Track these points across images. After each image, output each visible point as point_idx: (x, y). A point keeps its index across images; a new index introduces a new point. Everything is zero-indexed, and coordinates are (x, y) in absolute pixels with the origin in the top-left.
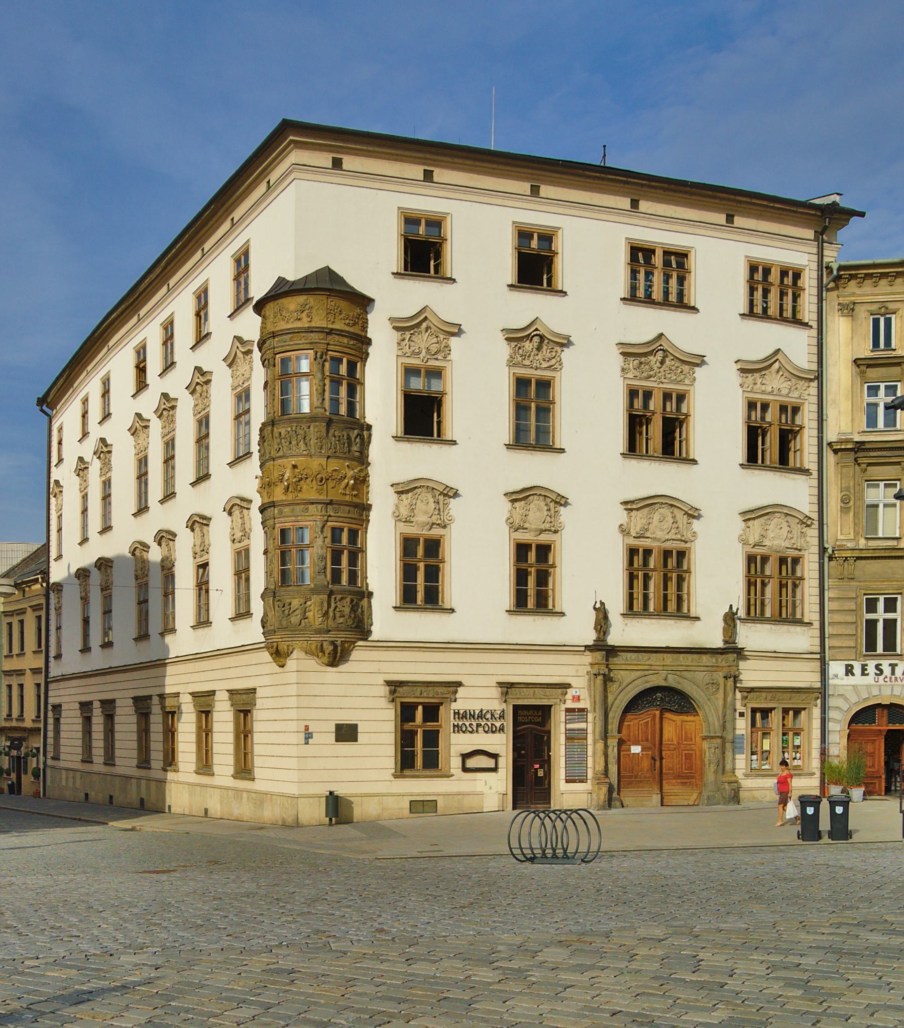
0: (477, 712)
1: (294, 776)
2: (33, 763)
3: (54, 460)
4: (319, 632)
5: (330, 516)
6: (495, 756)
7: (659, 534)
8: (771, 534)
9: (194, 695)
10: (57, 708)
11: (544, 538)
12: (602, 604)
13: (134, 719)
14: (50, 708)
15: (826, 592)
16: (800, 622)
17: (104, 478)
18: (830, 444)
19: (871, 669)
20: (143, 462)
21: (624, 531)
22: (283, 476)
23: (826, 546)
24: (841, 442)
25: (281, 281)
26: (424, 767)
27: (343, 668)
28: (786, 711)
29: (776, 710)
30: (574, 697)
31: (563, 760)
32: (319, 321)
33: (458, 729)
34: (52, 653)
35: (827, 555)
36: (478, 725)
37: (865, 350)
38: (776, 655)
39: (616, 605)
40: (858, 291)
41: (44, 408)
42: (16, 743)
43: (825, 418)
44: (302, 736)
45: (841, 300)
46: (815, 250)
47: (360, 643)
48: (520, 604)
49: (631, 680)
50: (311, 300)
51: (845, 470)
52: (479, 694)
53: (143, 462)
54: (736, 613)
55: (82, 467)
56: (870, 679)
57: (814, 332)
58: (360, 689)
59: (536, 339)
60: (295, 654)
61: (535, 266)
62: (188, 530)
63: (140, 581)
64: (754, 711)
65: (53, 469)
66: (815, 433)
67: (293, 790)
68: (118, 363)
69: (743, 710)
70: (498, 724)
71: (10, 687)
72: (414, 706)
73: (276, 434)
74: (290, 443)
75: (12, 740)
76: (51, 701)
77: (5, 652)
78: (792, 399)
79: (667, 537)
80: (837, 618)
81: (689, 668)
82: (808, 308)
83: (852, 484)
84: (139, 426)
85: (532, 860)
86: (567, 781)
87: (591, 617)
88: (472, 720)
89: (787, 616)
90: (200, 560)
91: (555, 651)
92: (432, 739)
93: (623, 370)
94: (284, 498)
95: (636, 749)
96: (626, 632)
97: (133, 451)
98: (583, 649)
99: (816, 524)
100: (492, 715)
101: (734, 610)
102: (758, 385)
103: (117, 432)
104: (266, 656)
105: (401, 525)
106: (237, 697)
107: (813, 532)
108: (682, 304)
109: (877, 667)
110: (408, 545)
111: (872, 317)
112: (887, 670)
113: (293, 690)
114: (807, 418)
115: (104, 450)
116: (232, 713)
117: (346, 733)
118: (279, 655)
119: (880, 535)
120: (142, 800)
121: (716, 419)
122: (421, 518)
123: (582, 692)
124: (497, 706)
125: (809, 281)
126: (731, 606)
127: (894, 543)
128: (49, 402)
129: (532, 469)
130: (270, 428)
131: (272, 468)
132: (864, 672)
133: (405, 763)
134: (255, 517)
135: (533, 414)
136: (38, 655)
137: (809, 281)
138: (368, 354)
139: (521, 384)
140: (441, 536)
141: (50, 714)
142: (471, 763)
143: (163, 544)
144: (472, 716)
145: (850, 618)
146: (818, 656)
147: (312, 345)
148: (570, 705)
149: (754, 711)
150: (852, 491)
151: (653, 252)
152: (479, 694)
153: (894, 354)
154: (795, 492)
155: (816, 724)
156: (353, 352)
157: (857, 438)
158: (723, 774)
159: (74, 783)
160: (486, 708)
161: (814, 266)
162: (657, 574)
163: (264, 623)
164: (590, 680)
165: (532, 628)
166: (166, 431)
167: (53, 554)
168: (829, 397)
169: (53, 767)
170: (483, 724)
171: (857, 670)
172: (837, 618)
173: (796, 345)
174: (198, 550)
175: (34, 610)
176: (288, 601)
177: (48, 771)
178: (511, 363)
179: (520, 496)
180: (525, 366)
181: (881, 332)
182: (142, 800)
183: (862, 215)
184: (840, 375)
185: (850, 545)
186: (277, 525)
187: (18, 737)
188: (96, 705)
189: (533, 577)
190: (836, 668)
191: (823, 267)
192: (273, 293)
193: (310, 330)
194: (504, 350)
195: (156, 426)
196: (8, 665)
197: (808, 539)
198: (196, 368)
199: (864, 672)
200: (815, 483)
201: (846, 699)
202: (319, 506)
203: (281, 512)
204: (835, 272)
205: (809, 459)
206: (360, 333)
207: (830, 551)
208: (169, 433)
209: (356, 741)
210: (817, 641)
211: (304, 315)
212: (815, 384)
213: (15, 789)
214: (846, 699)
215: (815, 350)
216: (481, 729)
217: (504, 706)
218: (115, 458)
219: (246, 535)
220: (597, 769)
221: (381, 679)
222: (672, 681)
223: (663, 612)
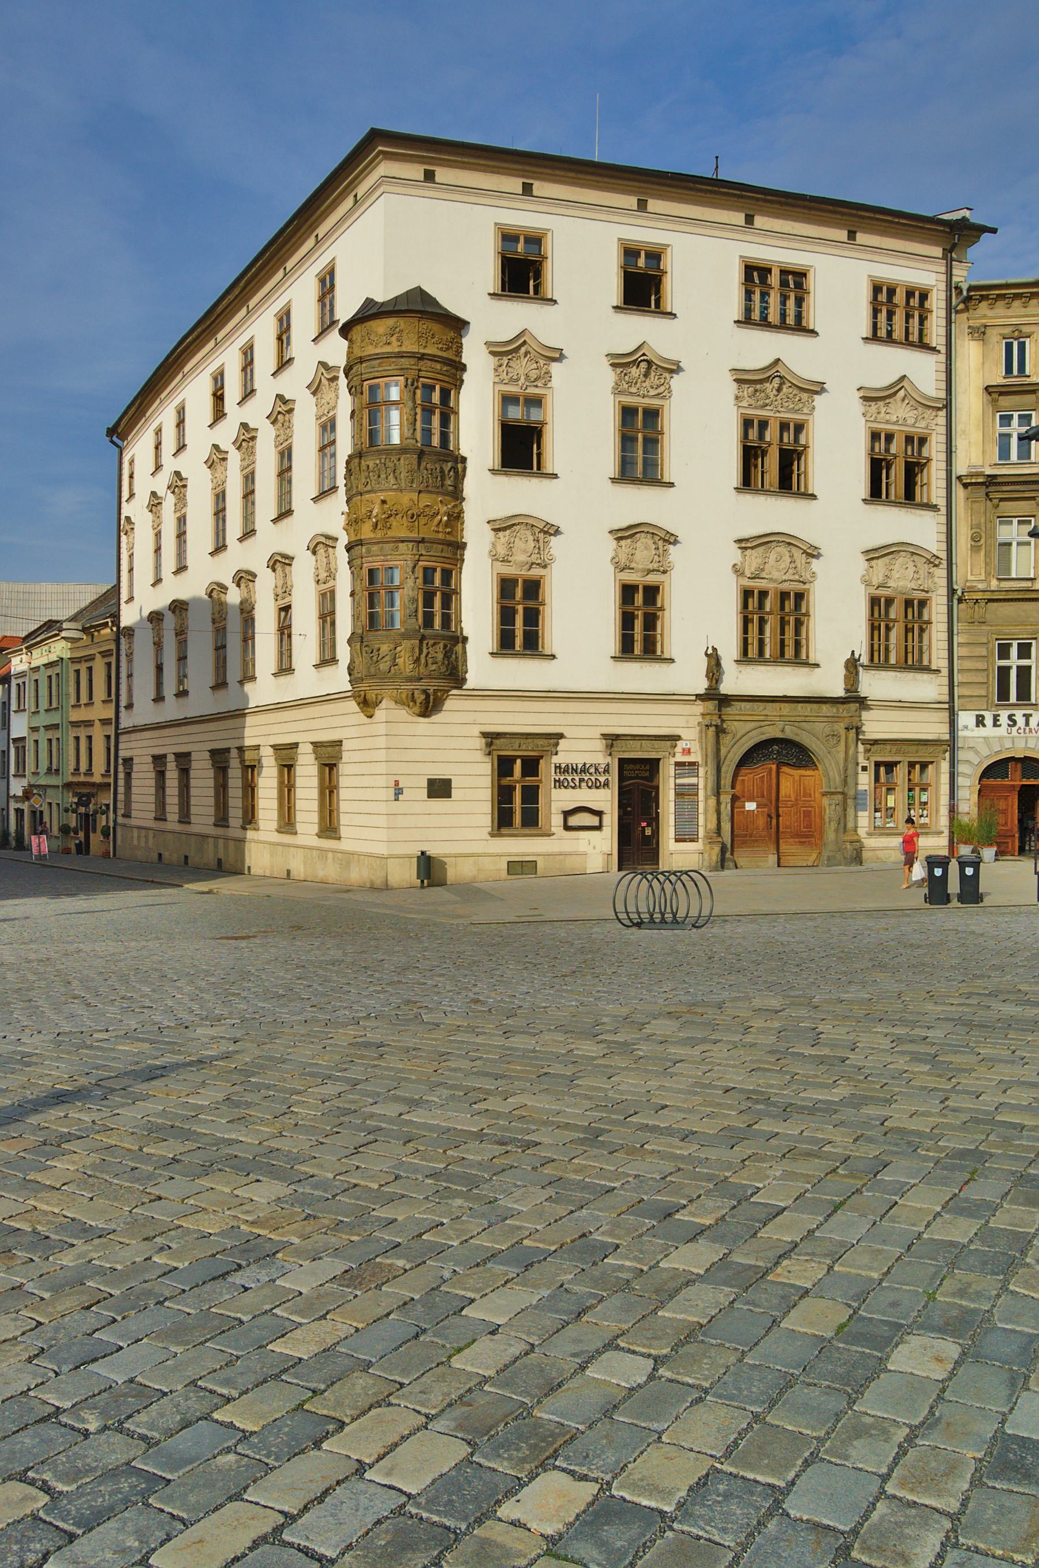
0: (580, 766)
2: (102, 821)
3: (125, 495)
4: (410, 679)
5: (421, 555)
6: (599, 814)
7: (776, 575)
10: (128, 761)
11: (652, 579)
12: (714, 649)
13: (211, 773)
14: (120, 761)
15: (955, 637)
16: (927, 669)
17: (178, 514)
18: (959, 478)
19: (1004, 720)
20: (220, 497)
21: (738, 571)
22: (371, 512)
23: (955, 587)
24: (971, 475)
25: (369, 302)
28: (912, 765)
29: (903, 764)
30: (684, 750)
31: (672, 817)
33: (559, 784)
34: (123, 703)
35: (956, 597)
36: (581, 780)
37: (997, 377)
38: (902, 704)
39: (729, 651)
40: (990, 313)
41: (115, 439)
43: (954, 449)
44: (392, 792)
45: (971, 323)
46: (943, 269)
47: (454, 692)
49: (745, 731)
50: (401, 323)
51: (975, 505)
52: (581, 747)
53: (220, 497)
54: (859, 660)
55: (155, 503)
56: (1002, 731)
57: (942, 358)
58: (454, 741)
59: (644, 365)
61: (642, 286)
62: (270, 570)
63: (217, 625)
64: (878, 765)
65: (124, 504)
67: (382, 849)
68: (193, 391)
69: (866, 763)
70: (602, 779)
73: (364, 468)
74: (379, 476)
75: (80, 796)
78: (919, 429)
79: (784, 578)
80: (968, 664)
81: (807, 719)
82: (936, 334)
83: (983, 520)
84: (217, 458)
86: (677, 840)
87: (703, 663)
88: (575, 775)
89: (913, 663)
90: (282, 603)
91: (663, 701)
92: (531, 795)
93: (737, 398)
95: (751, 806)
96: (737, 680)
97: (210, 486)
98: (694, 698)
100: (596, 769)
101: (857, 656)
102: (882, 415)
104: (352, 706)
107: (941, 573)
108: (800, 327)
109: (1010, 717)
110: (506, 586)
111: (1004, 341)
112: (1021, 721)
114: (935, 450)
115: (179, 484)
116: (316, 767)
117: (440, 789)
118: (367, 705)
119: (1014, 576)
120: (220, 861)
121: (836, 454)
122: (520, 557)
123: (692, 744)
124: (601, 759)
125: (937, 303)
126: (853, 652)
127: (1028, 584)
128: (120, 432)
129: (639, 504)
132: (996, 724)
133: (503, 821)
134: (341, 556)
135: (640, 445)
137: (937, 303)
139: (627, 413)
140: (541, 577)
141: (121, 768)
142: (573, 821)
143: (243, 585)
146: (946, 706)
147: (402, 371)
148: (680, 758)
149: (878, 765)
150: (983, 528)
151: (769, 271)
152: (581, 747)
154: (921, 529)
155: (945, 779)
156: (446, 379)
157: (989, 471)
159: (147, 842)
160: (589, 762)
161: (942, 286)
162: (774, 618)
163: (350, 670)
164: (701, 731)
165: (639, 676)
168: (958, 427)
169: (124, 825)
170: (586, 778)
171: (989, 721)
172: (968, 664)
173: (923, 371)
174: (280, 591)
176: (377, 646)
177: (119, 830)
178: (617, 391)
179: (625, 534)
181: (1014, 356)
182: (220, 861)
183: (994, 231)
184: (970, 402)
186: (365, 565)
190: (966, 719)
192: (360, 316)
193: (400, 355)
194: (609, 377)
195: (234, 458)
197: (936, 580)
198: (277, 395)
199: (996, 724)
200: (943, 519)
201: (977, 752)
202: (410, 545)
203: (369, 551)
204: (965, 293)
205: (937, 494)
207: (959, 593)
209: (429, 780)
210: (946, 690)
211: (394, 338)
214: (977, 752)
215: (943, 377)
216: (584, 784)
217: (609, 759)
218: (190, 493)
219: (331, 575)
220: (709, 827)
222: (790, 733)
223: (780, 658)
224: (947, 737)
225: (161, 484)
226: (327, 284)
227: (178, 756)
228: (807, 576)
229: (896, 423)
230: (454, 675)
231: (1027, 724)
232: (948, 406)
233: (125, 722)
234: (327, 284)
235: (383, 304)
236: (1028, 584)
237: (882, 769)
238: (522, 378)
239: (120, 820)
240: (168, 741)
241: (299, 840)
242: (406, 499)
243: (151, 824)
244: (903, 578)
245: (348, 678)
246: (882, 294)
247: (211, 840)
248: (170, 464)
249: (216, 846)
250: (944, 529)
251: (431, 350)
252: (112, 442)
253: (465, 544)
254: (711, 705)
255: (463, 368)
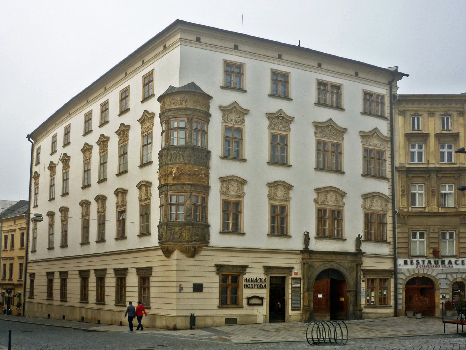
0: (254, 279)
1: (175, 307)
2: (16, 301)
3: (34, 163)
5: (193, 191)
6: (262, 299)
8: (374, 205)
9: (96, 270)
10: (32, 275)
11: (283, 203)
12: (308, 233)
13: (79, 280)
14: (28, 275)
15: (396, 230)
17: (64, 171)
18: (396, 168)
21: (316, 201)
22: (172, 172)
23: (396, 210)
24: (401, 167)
25: (171, 87)
26: (231, 303)
27: (197, 258)
28: (380, 280)
29: (378, 279)
30: (295, 273)
31: (290, 300)
32: (190, 106)
33: (247, 287)
34: (30, 249)
36: (255, 285)
37: (410, 131)
38: (377, 255)
39: (313, 234)
42: (9, 291)
44: (178, 289)
45: (400, 109)
46: (389, 89)
47: (205, 248)
48: (273, 233)
49: (319, 266)
51: (403, 179)
52: (255, 272)
54: (361, 238)
55: (52, 167)
56: (414, 267)
57: (389, 122)
58: (203, 269)
59: (281, 118)
60: (176, 252)
63: (84, 218)
64: (368, 279)
65: (34, 167)
66: (390, 163)
67: (174, 313)
68: (76, 121)
69: (364, 279)
70: (263, 285)
71: (5, 265)
72: (227, 276)
73: (170, 154)
74: (176, 158)
75: (7, 290)
76: (29, 271)
77: (3, 248)
80: (401, 240)
83: (406, 184)
84: (87, 149)
85: (315, 343)
89: (381, 240)
90: (120, 209)
91: (287, 252)
92: (235, 291)
93: (315, 133)
94: (172, 182)
95: (320, 296)
96: (317, 245)
99: (391, 201)
100: (261, 280)
102: (368, 142)
103: (75, 152)
104: (160, 252)
105: (222, 196)
106: (98, 273)
107: (390, 204)
109: (417, 261)
110: (226, 204)
112: (421, 263)
113: (175, 268)
114: (388, 156)
115: (66, 160)
116: (138, 278)
117: (198, 288)
118: (168, 253)
119: (417, 206)
120: (83, 318)
121: (353, 154)
124: (263, 276)
126: (359, 235)
127: (423, 210)
129: (278, 174)
130: (166, 151)
131: (167, 169)
132: (412, 263)
134: (155, 191)
136: (22, 251)
138: (210, 120)
139: (274, 137)
140: (240, 201)
141: (28, 278)
142: (253, 301)
144: (252, 281)
145: (406, 241)
146: (393, 256)
147: (187, 116)
148: (293, 276)
149: (368, 279)
152: (255, 272)
153: (450, 132)
154: (383, 188)
155: (392, 285)
156: (204, 119)
157: (407, 166)
158: (356, 306)
159: (42, 310)
161: (388, 95)
162: (330, 221)
164: (302, 266)
165: (278, 243)
166: (102, 151)
167: (32, 205)
168: (396, 148)
169: (30, 302)
172: (401, 240)
175: (20, 230)
176: (173, 228)
177: (26, 305)
178: (270, 128)
180: (276, 129)
182: (83, 318)
184: (400, 139)
185: (406, 210)
186: (169, 194)
187: (10, 288)
188: (92, 272)
189: (279, 224)
190: (400, 262)
191: (393, 97)
192: (169, 92)
193: (186, 109)
196: (4, 255)
197: (388, 207)
198: (121, 124)
199: (412, 263)
200: (390, 184)
201: (405, 275)
202: (189, 186)
205: (388, 174)
206: (206, 111)
207: (398, 212)
208: (103, 152)
210: (392, 250)
211: (183, 103)
212: (389, 143)
213: (8, 312)
214: (405, 275)
216: (256, 287)
217: (266, 277)
218: (71, 163)
219: (148, 198)
220: (305, 304)
221: (213, 264)
222: (335, 266)
223: (330, 237)
224: (393, 269)
225: (56, 158)
226: (148, 80)
227: (61, 273)
228: (341, 204)
229: (373, 146)
230: (205, 239)
231: (423, 263)
232: (391, 140)
233: (31, 257)
234: (148, 80)
235: (179, 88)
236: (423, 210)
237: (382, 281)
238: (233, 121)
239: (27, 300)
240: (42, 267)
241: (107, 307)
242: (188, 167)
243: (46, 302)
244: (377, 206)
245: (158, 241)
246: (368, 96)
247: (78, 309)
248: (61, 150)
249: (81, 312)
250: (390, 187)
251: (199, 108)
252: (29, 140)
253: (210, 187)
254: (306, 255)
255: (210, 115)
